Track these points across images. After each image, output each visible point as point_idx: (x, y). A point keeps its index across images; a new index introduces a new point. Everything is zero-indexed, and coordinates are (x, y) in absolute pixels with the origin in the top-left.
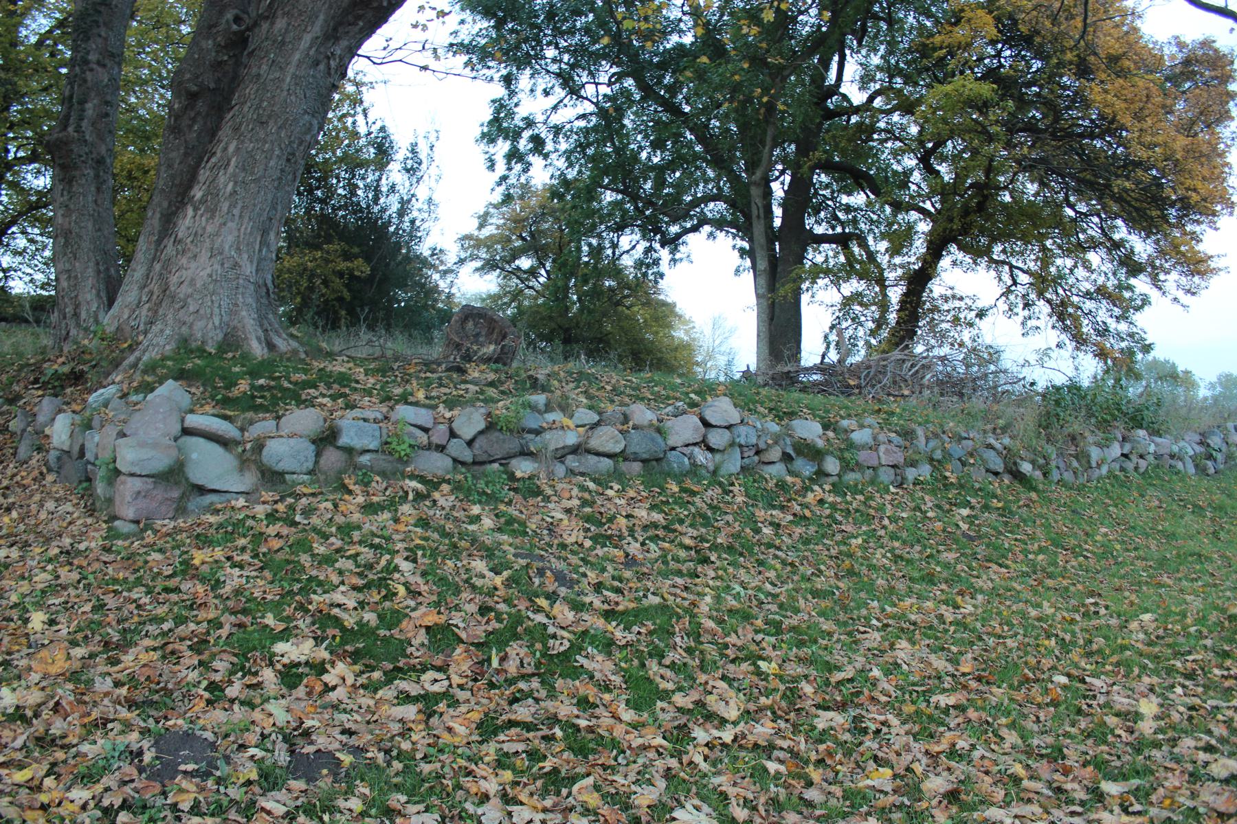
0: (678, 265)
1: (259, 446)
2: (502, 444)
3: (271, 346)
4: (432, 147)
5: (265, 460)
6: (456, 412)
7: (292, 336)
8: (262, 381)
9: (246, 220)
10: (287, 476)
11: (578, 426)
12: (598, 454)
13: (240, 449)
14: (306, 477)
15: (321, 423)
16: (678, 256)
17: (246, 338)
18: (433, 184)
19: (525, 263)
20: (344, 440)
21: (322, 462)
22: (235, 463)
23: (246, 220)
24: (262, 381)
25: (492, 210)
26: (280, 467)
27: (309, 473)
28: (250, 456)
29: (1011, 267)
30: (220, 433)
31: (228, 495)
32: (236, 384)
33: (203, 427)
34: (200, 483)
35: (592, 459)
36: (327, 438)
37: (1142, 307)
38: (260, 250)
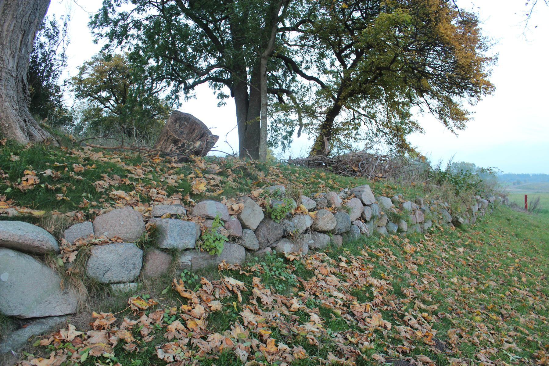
0: (190, 100)
1: (84, 253)
2: (273, 231)
3: (30, 136)
4: (65, 24)
5: (91, 273)
6: (241, 205)
7: (42, 126)
8: (48, 172)
9: (9, 18)
10: (114, 287)
11: (309, 211)
12: (325, 232)
13: (61, 262)
14: (132, 285)
15: (143, 224)
16: (188, 95)
17: (10, 127)
18: (65, 46)
19: (104, 94)
20: (168, 242)
21: (148, 266)
22: (57, 279)
23: (9, 18)
24: (48, 172)
25: (87, 66)
26: (105, 279)
27: (136, 280)
28: (73, 269)
29: (354, 110)
30: (36, 243)
31: (51, 322)
32: (22, 175)
33: (16, 239)
34: (15, 313)
35: (321, 236)
36: (151, 240)
37: (409, 133)
38: (20, 50)
